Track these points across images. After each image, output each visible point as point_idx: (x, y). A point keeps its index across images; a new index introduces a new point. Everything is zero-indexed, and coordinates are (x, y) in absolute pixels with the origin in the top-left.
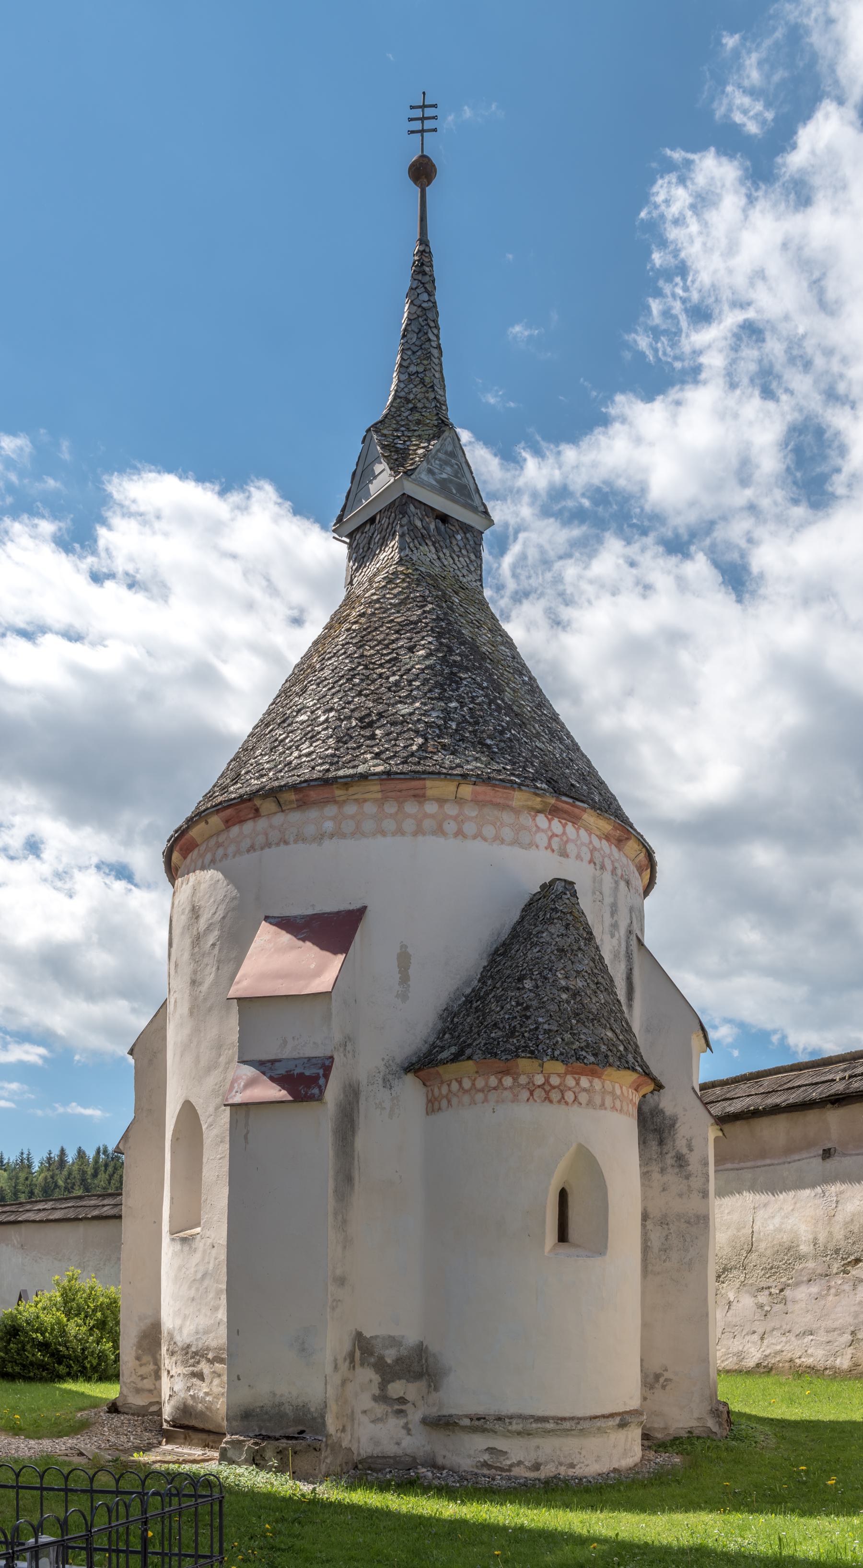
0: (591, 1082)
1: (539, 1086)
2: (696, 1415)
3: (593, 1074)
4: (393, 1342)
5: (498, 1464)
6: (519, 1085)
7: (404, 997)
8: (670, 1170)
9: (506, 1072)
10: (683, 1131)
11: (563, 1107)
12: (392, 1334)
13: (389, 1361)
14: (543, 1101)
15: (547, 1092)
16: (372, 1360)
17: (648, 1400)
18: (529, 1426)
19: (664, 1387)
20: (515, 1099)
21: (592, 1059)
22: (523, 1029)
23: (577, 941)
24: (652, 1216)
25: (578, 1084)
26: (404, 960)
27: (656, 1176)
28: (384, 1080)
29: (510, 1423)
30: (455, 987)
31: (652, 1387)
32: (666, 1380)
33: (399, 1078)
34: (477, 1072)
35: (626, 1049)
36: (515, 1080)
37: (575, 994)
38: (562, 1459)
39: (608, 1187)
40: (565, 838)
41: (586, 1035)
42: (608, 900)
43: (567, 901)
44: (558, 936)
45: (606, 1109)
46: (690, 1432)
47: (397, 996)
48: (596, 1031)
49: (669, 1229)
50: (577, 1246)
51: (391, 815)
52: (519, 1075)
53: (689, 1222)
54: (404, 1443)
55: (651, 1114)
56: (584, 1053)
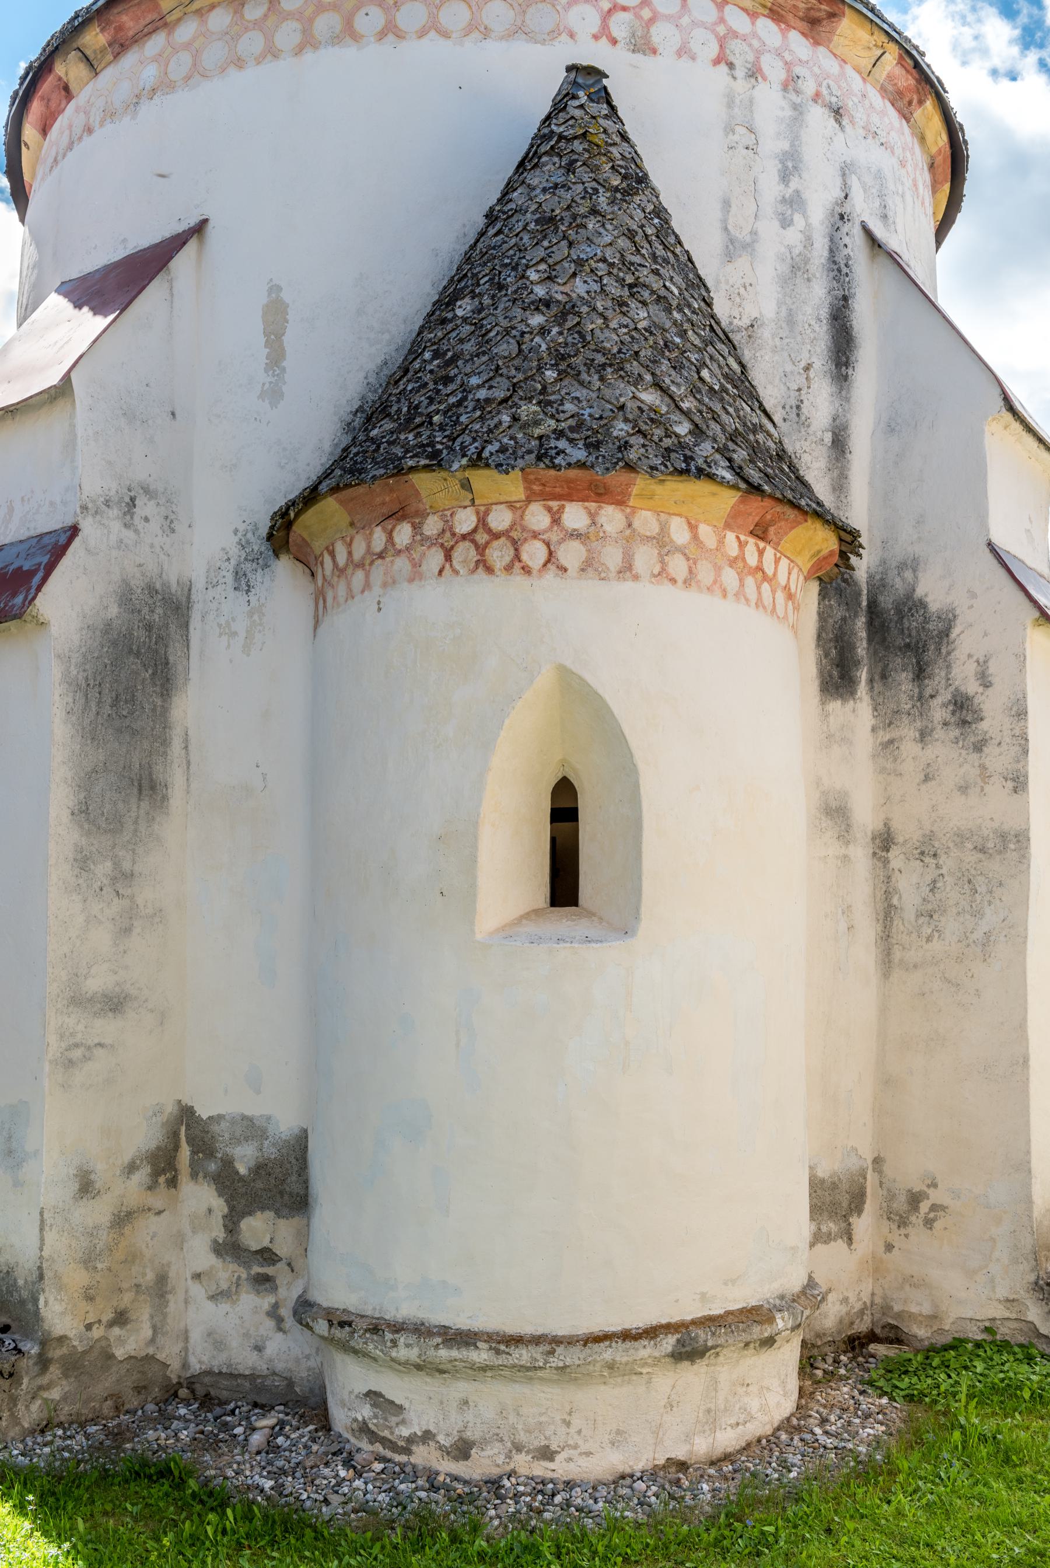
0: (593, 516)
1: (464, 537)
2: (1002, 1292)
3: (600, 494)
4: (252, 1128)
5: (386, 1433)
6: (425, 539)
7: (274, 394)
8: (939, 733)
9: (398, 514)
10: (967, 644)
11: (518, 579)
12: (248, 1113)
13: (242, 1170)
14: (473, 571)
15: (480, 549)
16: (213, 1167)
17: (895, 1251)
18: (432, 1352)
19: (929, 1223)
20: (416, 575)
21: (579, 454)
22: (433, 408)
23: (586, 195)
24: (901, 839)
25: (556, 521)
26: (275, 316)
27: (910, 748)
28: (239, 575)
29: (394, 1343)
30: (379, 361)
31: (903, 1223)
32: (934, 1208)
33: (266, 566)
34: (352, 524)
35: (698, 431)
36: (416, 528)
37: (567, 310)
38: (522, 1437)
39: (641, 766)
40: (646, 14)
41: (579, 401)
42: (772, 144)
43: (578, 113)
44: (544, 190)
45: (636, 578)
46: (987, 1330)
47: (262, 396)
48: (607, 393)
49: (938, 866)
50: (590, 914)
51: (255, 23)
52: (423, 515)
53: (983, 850)
54: (271, 1349)
55: (899, 611)
56: (562, 444)
